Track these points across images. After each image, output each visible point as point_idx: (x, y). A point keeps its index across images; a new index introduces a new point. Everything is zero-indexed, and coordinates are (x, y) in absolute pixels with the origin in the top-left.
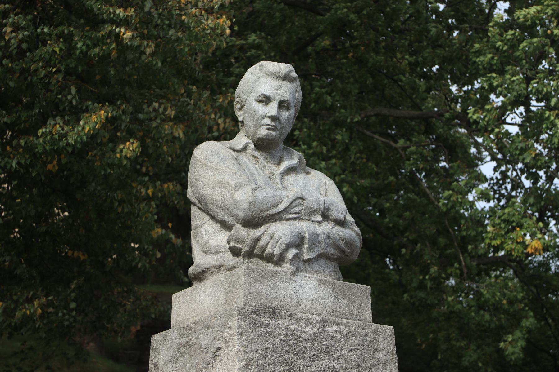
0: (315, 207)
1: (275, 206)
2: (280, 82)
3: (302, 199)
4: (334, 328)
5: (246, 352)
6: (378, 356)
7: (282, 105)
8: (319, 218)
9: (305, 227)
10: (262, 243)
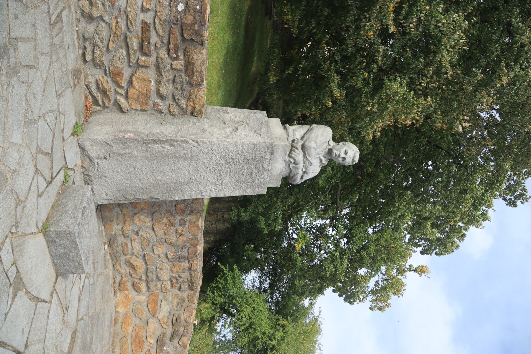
0: (308, 169)
5: (259, 144)
8: (304, 170)
9: (301, 165)
10: (296, 150)
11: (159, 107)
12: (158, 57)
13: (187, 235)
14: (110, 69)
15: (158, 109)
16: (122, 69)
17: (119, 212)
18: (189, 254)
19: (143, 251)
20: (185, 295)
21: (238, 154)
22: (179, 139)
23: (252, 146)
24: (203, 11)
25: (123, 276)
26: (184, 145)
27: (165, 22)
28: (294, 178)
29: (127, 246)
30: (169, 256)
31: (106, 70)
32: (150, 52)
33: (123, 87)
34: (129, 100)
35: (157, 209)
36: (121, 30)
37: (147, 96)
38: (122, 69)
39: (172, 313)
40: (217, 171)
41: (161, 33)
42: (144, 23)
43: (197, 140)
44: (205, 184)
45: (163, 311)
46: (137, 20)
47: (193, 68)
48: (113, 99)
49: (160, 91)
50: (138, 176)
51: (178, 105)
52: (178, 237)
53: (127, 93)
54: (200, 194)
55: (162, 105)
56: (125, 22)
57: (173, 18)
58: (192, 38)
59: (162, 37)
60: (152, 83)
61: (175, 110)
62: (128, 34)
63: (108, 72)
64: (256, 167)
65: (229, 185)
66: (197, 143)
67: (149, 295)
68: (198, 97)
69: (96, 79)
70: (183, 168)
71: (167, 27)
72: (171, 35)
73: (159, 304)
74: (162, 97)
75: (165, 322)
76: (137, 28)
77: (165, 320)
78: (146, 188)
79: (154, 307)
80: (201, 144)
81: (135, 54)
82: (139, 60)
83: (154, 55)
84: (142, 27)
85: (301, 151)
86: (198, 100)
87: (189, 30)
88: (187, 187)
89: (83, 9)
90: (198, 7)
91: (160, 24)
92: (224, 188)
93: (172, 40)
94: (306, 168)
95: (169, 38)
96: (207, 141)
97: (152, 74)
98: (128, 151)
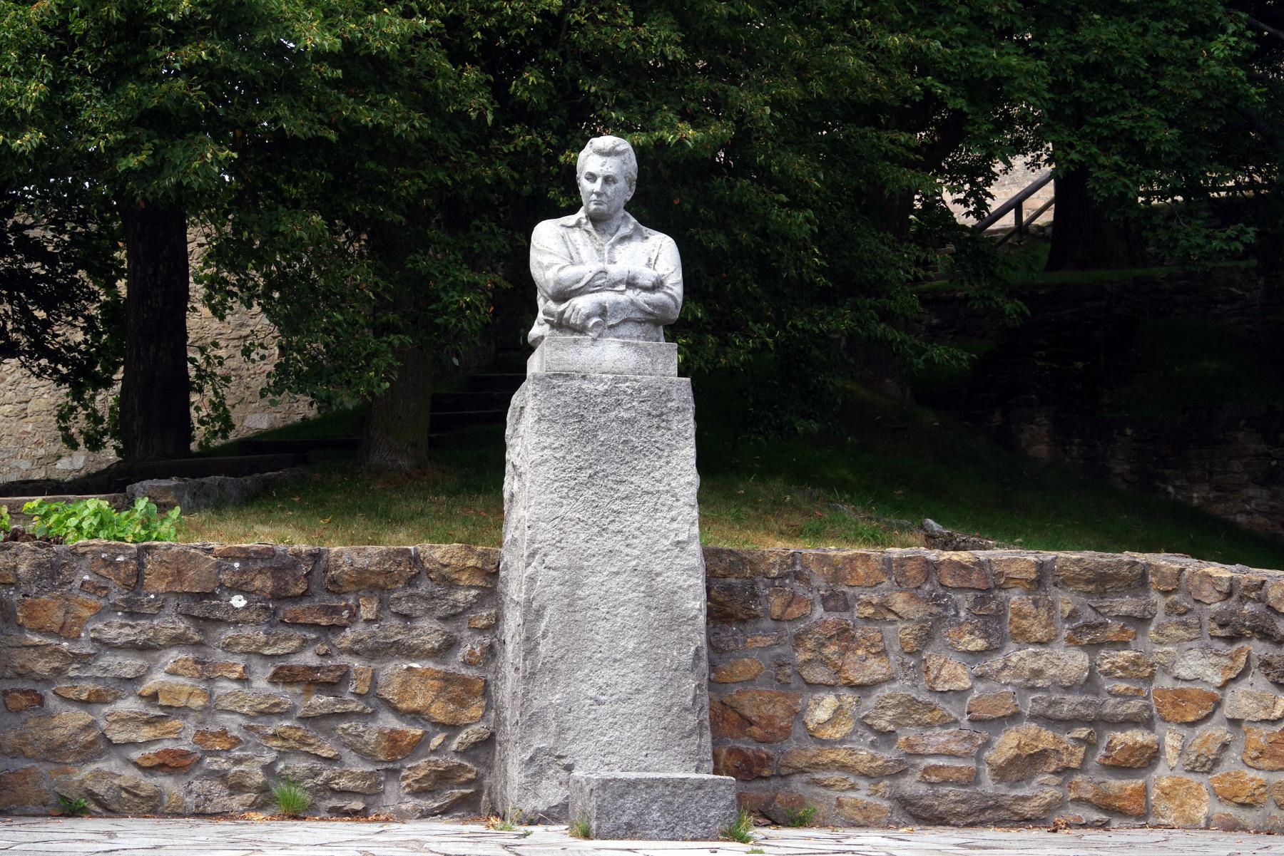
0: (618, 278)
1: (578, 282)
2: (605, 159)
3: (606, 273)
4: (627, 384)
5: (539, 410)
6: (670, 404)
7: (608, 180)
8: (622, 287)
9: (608, 297)
10: (566, 315)
11: (478, 651)
12: (352, 652)
13: (888, 590)
14: (382, 758)
15: (482, 654)
16: (381, 732)
17: (805, 778)
18: (966, 585)
19: (956, 721)
20: (1161, 602)
21: (564, 458)
22: (524, 597)
23: (545, 425)
24: (243, 555)
25: (1072, 795)
26: (539, 583)
27: (269, 634)
28: (650, 309)
29: (937, 768)
30: (979, 644)
31: (386, 770)
32: (339, 667)
33: (425, 733)
34: (461, 722)
35: (788, 671)
36: (291, 728)
37: (448, 679)
38: (381, 732)
39: (1208, 640)
40: (613, 507)
41: (295, 643)
42: (276, 679)
43: (526, 554)
44: (651, 535)
45: (1200, 670)
46: (267, 693)
47: (372, 572)
48: (457, 760)
49: (433, 648)
50: (623, 696)
51: (470, 607)
52: (895, 618)
53: (442, 726)
54: (684, 546)
55: (471, 645)
56: (275, 719)
57: (261, 618)
58: (305, 576)
59: (305, 641)
60: (415, 665)
61: (483, 616)
62: (299, 714)
63: (391, 766)
64: (604, 411)
65: (657, 475)
66: (532, 555)
67: (1163, 719)
68: (445, 561)
69: (407, 794)
70: (604, 588)
71: (282, 630)
72: (300, 621)
73: (1184, 686)
74: (450, 645)
75: (1230, 663)
76: (286, 695)
77: (1225, 661)
78: (662, 678)
79: (1191, 700)
80: (536, 546)
81: (345, 702)
82: (358, 691)
83: (345, 659)
84: (284, 683)
85: (567, 303)
86: (453, 561)
87: (287, 583)
88: (659, 579)
89: (249, 802)
90: (237, 565)
91: (275, 644)
92: (668, 488)
93: (310, 620)
94: (615, 284)
95: (305, 625)
96: (530, 532)
97: (393, 668)
98: (551, 715)
